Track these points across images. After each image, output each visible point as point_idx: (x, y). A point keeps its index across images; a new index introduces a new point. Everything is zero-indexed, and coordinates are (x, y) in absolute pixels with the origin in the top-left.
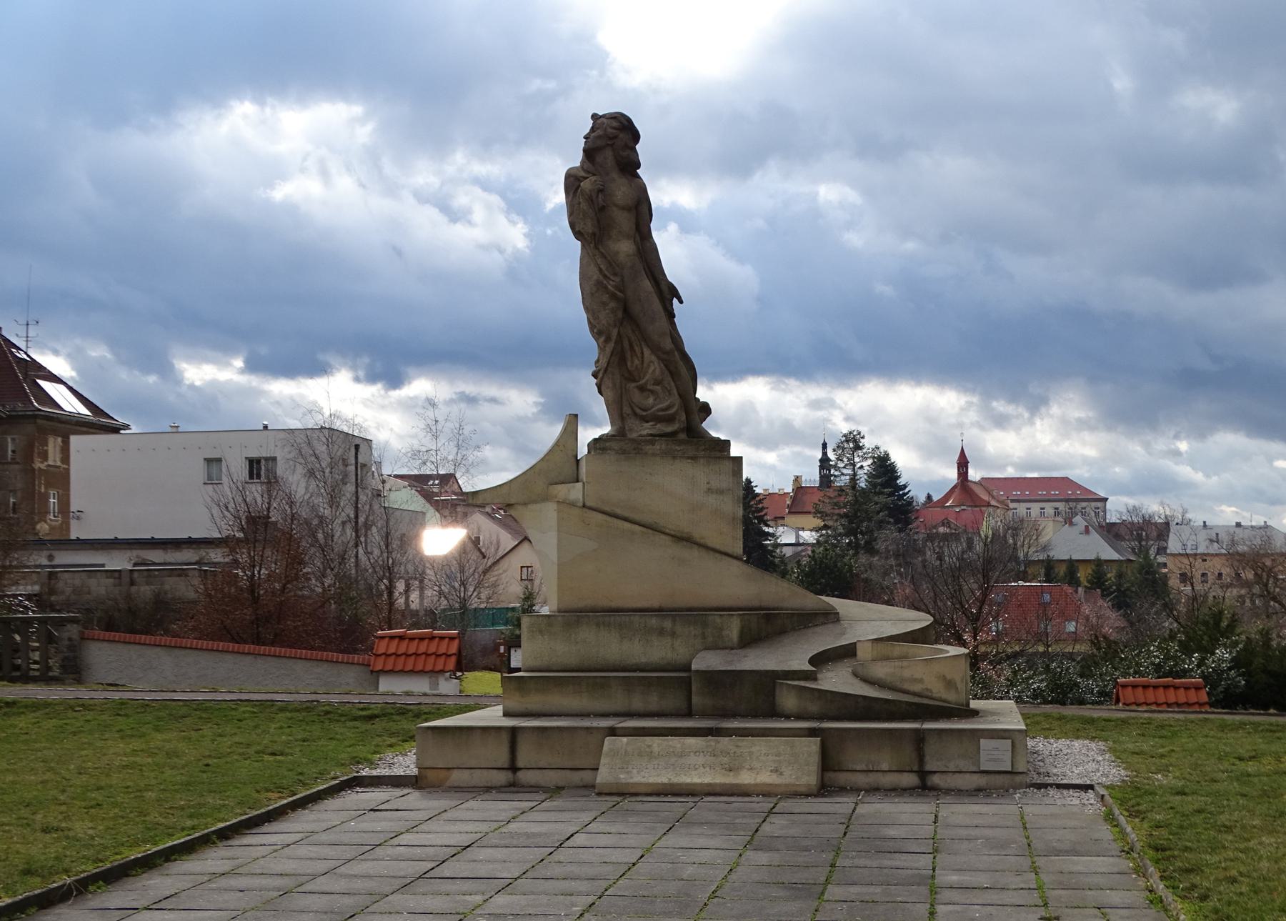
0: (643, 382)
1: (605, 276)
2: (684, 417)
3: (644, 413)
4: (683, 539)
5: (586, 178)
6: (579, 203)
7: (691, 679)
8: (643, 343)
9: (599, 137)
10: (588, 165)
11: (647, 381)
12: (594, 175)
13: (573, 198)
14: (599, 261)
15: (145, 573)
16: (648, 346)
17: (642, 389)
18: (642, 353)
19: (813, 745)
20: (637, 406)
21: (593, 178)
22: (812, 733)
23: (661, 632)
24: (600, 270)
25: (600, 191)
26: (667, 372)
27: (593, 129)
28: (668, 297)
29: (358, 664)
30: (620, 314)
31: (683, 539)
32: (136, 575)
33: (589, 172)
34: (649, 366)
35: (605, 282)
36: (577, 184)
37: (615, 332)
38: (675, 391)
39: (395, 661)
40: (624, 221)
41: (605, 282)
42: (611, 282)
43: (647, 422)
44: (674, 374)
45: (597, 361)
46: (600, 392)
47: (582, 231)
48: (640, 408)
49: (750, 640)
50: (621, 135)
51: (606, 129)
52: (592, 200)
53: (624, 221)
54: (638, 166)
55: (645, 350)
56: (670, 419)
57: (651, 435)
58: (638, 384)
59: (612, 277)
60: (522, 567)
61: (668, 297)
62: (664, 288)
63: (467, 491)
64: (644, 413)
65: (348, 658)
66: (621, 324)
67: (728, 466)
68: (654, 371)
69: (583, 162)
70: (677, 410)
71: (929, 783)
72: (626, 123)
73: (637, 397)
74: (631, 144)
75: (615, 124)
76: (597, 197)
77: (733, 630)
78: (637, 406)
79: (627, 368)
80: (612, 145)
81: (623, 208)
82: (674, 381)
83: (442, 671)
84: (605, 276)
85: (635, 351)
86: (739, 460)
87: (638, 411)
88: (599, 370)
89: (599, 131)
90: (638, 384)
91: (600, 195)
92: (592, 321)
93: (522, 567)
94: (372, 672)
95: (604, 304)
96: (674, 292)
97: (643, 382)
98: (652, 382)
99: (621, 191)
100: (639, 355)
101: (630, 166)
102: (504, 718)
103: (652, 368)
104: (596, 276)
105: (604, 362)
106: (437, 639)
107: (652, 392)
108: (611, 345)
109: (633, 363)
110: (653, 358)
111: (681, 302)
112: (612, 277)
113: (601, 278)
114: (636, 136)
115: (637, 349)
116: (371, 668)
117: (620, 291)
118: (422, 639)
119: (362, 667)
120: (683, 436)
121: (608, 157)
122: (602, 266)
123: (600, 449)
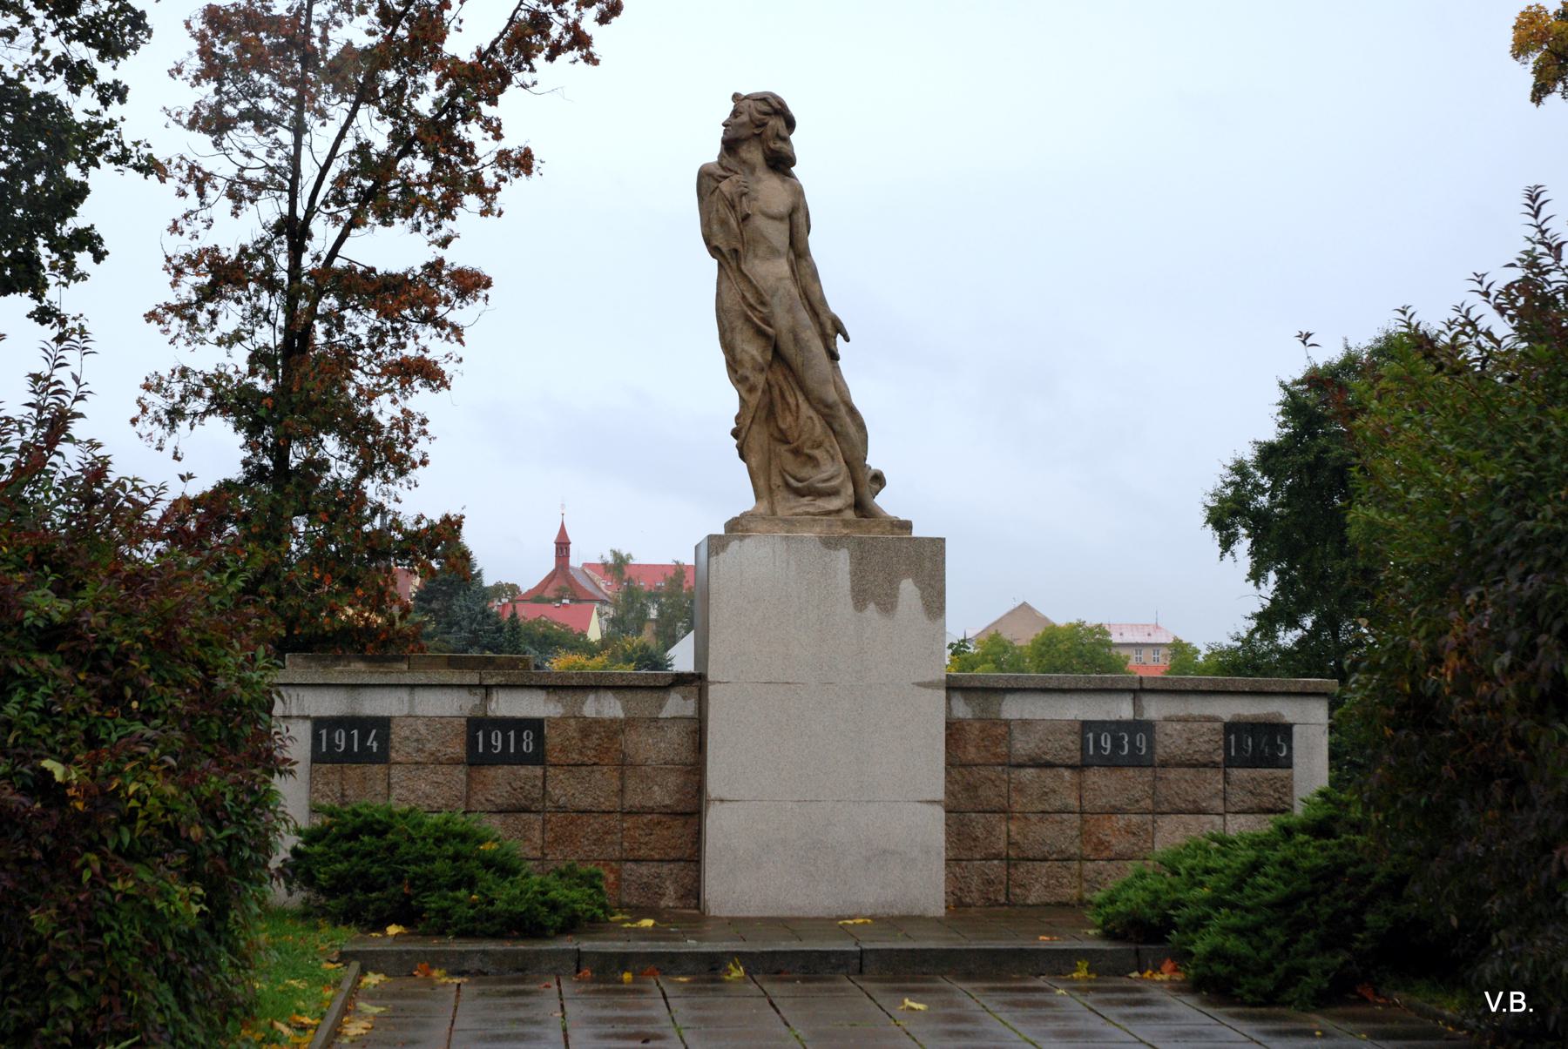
1: (750, 306)
17: (796, 452)
43: (803, 496)
59: (759, 307)
62: (824, 318)
70: (843, 482)
76: (741, 201)
84: (750, 306)
110: (812, 413)
111: (847, 340)
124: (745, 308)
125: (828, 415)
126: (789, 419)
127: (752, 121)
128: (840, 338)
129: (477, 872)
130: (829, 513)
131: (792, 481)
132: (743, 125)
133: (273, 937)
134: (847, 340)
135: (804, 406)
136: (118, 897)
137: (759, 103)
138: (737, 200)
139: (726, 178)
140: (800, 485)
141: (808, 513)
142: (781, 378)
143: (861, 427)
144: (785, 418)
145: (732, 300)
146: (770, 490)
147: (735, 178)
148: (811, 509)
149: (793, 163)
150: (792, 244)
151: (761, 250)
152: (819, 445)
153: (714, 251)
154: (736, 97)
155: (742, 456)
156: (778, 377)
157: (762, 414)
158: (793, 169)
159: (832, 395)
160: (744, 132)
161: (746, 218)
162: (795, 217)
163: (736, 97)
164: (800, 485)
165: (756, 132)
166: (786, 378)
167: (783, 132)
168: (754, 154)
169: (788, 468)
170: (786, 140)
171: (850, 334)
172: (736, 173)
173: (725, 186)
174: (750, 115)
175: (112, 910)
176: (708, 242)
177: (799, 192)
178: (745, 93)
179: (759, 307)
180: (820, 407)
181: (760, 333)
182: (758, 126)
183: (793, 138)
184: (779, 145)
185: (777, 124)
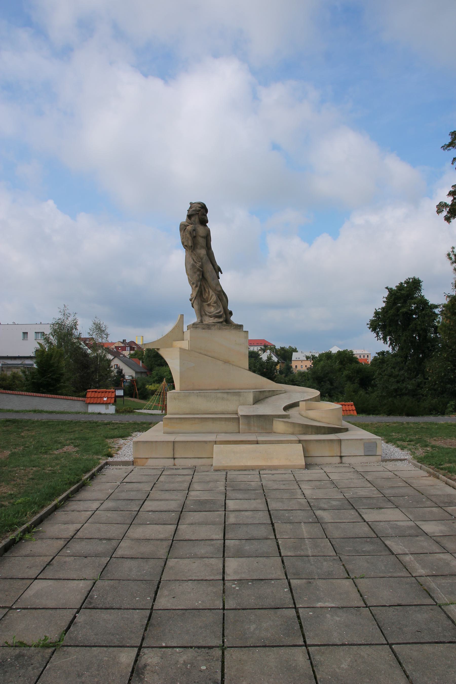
0: (209, 303)
1: (195, 262)
2: (225, 316)
3: (210, 314)
4: (226, 362)
5: (188, 225)
6: (186, 235)
7: (239, 418)
8: (209, 288)
9: (194, 210)
10: (189, 221)
11: (211, 302)
12: (191, 224)
13: (183, 232)
14: (193, 257)
15: (7, 368)
16: (211, 289)
18: (209, 292)
19: (300, 446)
20: (207, 312)
21: (192, 225)
22: (300, 441)
23: (223, 399)
24: (193, 260)
25: (194, 230)
26: (218, 299)
27: (191, 208)
28: (218, 271)
29: (81, 401)
30: (201, 277)
31: (226, 362)
32: (3, 368)
33: (189, 223)
34: (212, 297)
35: (195, 264)
36: (185, 228)
37: (199, 283)
38: (221, 306)
39: (90, 400)
40: (201, 241)
41: (195, 264)
42: (198, 264)
43: (211, 318)
44: (221, 300)
45: (192, 294)
46: (193, 306)
47: (187, 245)
48: (208, 313)
49: (257, 401)
50: (202, 210)
51: (196, 208)
52: (191, 234)
53: (201, 241)
54: (207, 222)
55: (210, 290)
56: (220, 317)
57: (214, 323)
58: (207, 303)
59: (198, 263)
60: (115, 365)
61: (218, 271)
62: (216, 267)
63: (334, 347)
64: (210, 314)
65: (78, 399)
66: (201, 280)
67: (242, 334)
68: (214, 298)
69: (187, 220)
70: (223, 314)
71: (343, 462)
72: (203, 206)
74: (205, 213)
75: (200, 206)
76: (193, 232)
77: (250, 398)
78: (207, 312)
79: (203, 298)
80: (198, 214)
81: (202, 237)
82: (221, 302)
83: (110, 403)
84: (195, 262)
85: (206, 291)
86: (247, 332)
87: (207, 313)
88: (193, 298)
89: (193, 208)
90: (207, 303)
91: (194, 232)
92: (190, 279)
93: (115, 365)
94: (86, 403)
95: (195, 273)
96: (219, 270)
97: (209, 303)
98: (213, 303)
99: (201, 229)
100: (208, 293)
101: (204, 222)
102: (117, 414)
104: (192, 262)
105: (195, 294)
106: (108, 392)
108: (197, 288)
109: (205, 296)
110: (213, 293)
111: (222, 273)
112: (198, 263)
113: (194, 263)
114: (206, 211)
115: (207, 290)
116: (86, 402)
117: (202, 268)
118: (103, 392)
119: (82, 402)
120: (224, 323)
121: (196, 219)
122: (194, 259)
123: (194, 327)
128: (220, 273)
134: (222, 273)
165: (197, 213)
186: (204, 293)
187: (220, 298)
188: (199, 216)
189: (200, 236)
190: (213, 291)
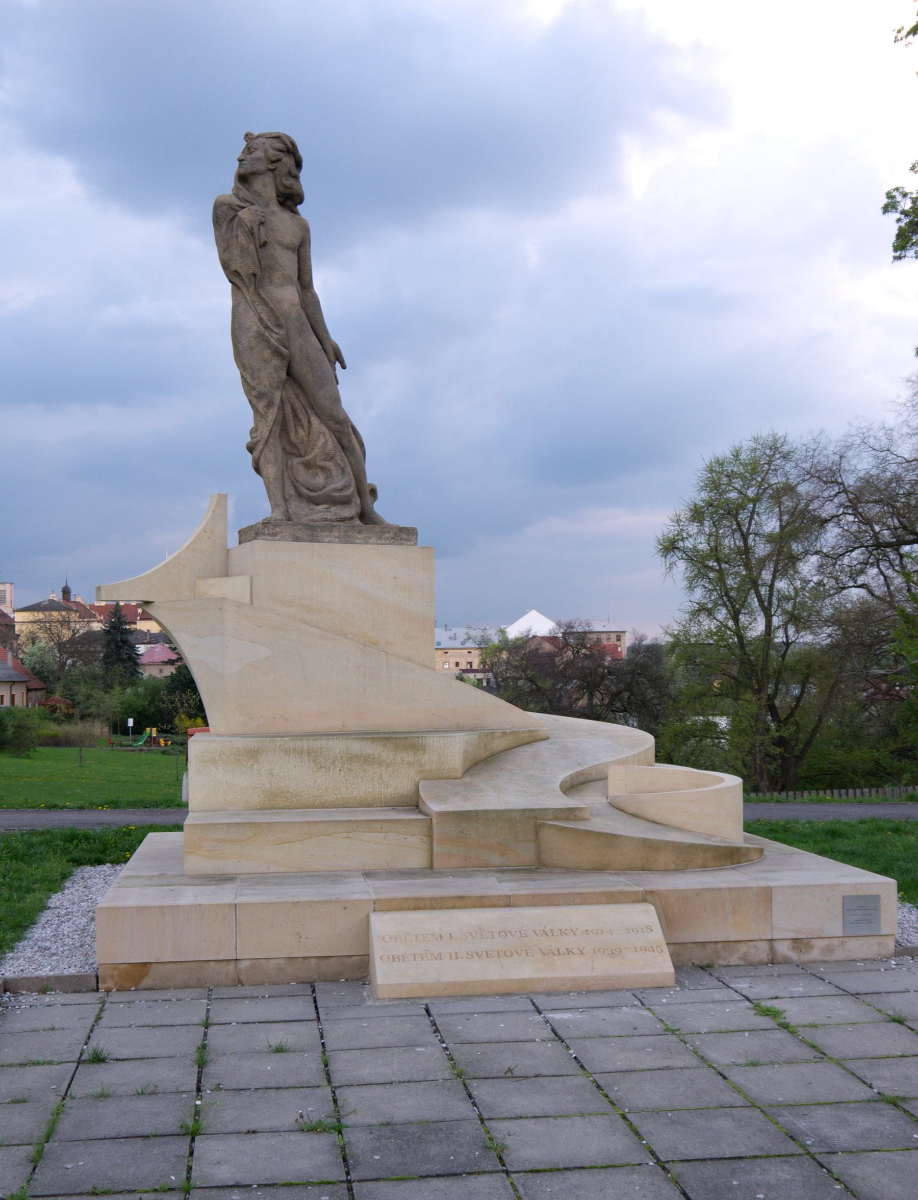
0: (308, 458)
1: (267, 328)
2: (358, 501)
16: (316, 414)
17: (308, 465)
18: (309, 422)
24: (261, 319)
43: (317, 504)
73: (303, 475)
76: (259, 230)
84: (267, 328)
100: (306, 424)
103: (322, 440)
107: (323, 469)
110: (324, 429)
111: (344, 367)
124: (263, 329)
125: (339, 432)
126: (302, 433)
127: (267, 158)
128: (338, 365)
129: (781, 733)
130: (343, 520)
131: (305, 491)
132: (258, 160)
133: (864, 915)
134: (344, 367)
135: (315, 421)
136: (19, 836)
137: (274, 141)
138: (255, 230)
139: (243, 208)
140: (315, 494)
141: (326, 520)
142: (293, 396)
143: (362, 445)
144: (297, 433)
145: (251, 322)
146: (286, 500)
147: (253, 208)
148: (329, 516)
149: (301, 201)
150: (299, 278)
151: (276, 277)
152: (331, 458)
153: (233, 275)
154: (248, 137)
155: (257, 469)
156: (291, 393)
157: (277, 429)
158: (299, 207)
159: (341, 417)
160: (261, 166)
161: (264, 245)
162: (302, 250)
163: (248, 137)
164: (315, 494)
166: (297, 397)
167: (294, 171)
168: (266, 187)
169: (300, 479)
170: (296, 178)
171: (347, 362)
172: (252, 204)
173: (244, 214)
174: (266, 151)
175: (893, 758)
176: (225, 266)
177: (305, 229)
178: (256, 133)
179: (275, 330)
180: (332, 423)
181: (277, 353)
182: (273, 162)
183: (304, 175)
184: (289, 182)
185: (288, 161)
186: (293, 428)
187: (345, 442)
188: (275, 178)
189: (279, 243)
190: (322, 421)
